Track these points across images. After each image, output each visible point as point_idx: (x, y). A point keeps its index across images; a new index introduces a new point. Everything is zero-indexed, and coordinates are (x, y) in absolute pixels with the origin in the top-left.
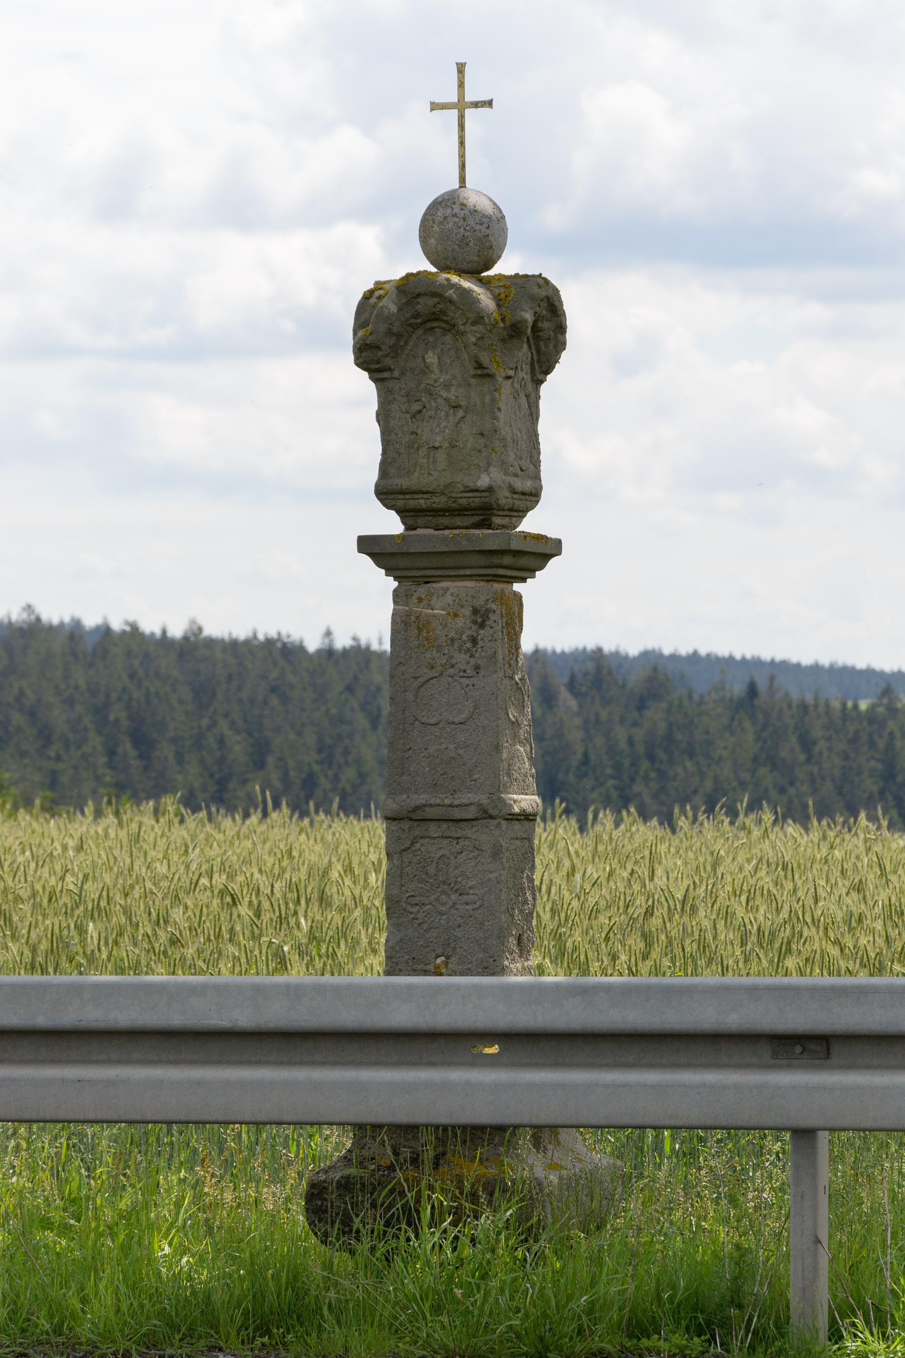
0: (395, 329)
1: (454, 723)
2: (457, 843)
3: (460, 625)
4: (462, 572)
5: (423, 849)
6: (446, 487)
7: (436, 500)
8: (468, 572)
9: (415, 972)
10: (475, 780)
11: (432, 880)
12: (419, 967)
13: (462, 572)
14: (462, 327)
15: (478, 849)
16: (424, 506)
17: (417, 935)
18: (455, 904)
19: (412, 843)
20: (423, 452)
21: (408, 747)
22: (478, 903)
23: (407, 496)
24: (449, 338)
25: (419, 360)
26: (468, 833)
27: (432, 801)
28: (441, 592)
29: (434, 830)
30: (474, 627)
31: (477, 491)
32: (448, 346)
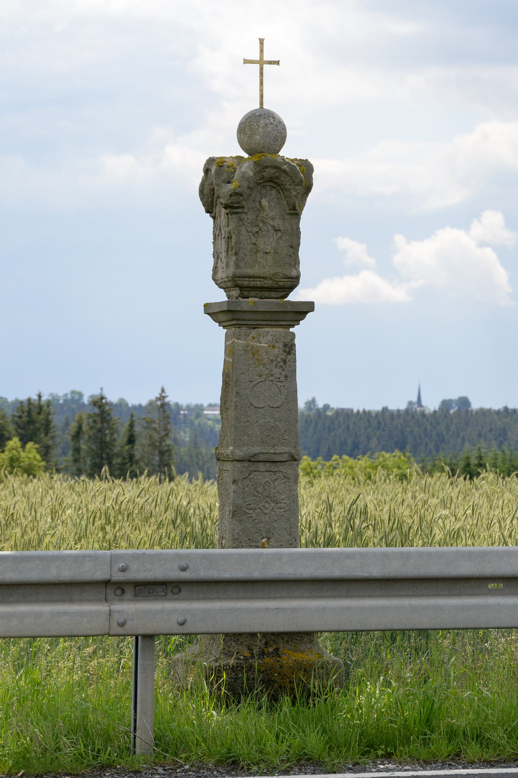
0: (251, 185)
1: (273, 407)
2: (274, 475)
3: (276, 352)
4: (280, 323)
5: (255, 477)
6: (274, 275)
7: (267, 282)
8: (283, 323)
9: (251, 547)
10: (285, 439)
11: (260, 495)
12: (253, 544)
13: (280, 323)
14: (288, 187)
15: (286, 478)
16: (259, 285)
17: (251, 526)
18: (273, 508)
19: (249, 475)
20: (259, 255)
21: (247, 420)
22: (287, 508)
23: (251, 279)
24: (274, 192)
25: (257, 204)
26: (282, 469)
27: (264, 451)
28: (265, 334)
29: (262, 467)
30: (284, 354)
31: (291, 278)
32: (273, 197)
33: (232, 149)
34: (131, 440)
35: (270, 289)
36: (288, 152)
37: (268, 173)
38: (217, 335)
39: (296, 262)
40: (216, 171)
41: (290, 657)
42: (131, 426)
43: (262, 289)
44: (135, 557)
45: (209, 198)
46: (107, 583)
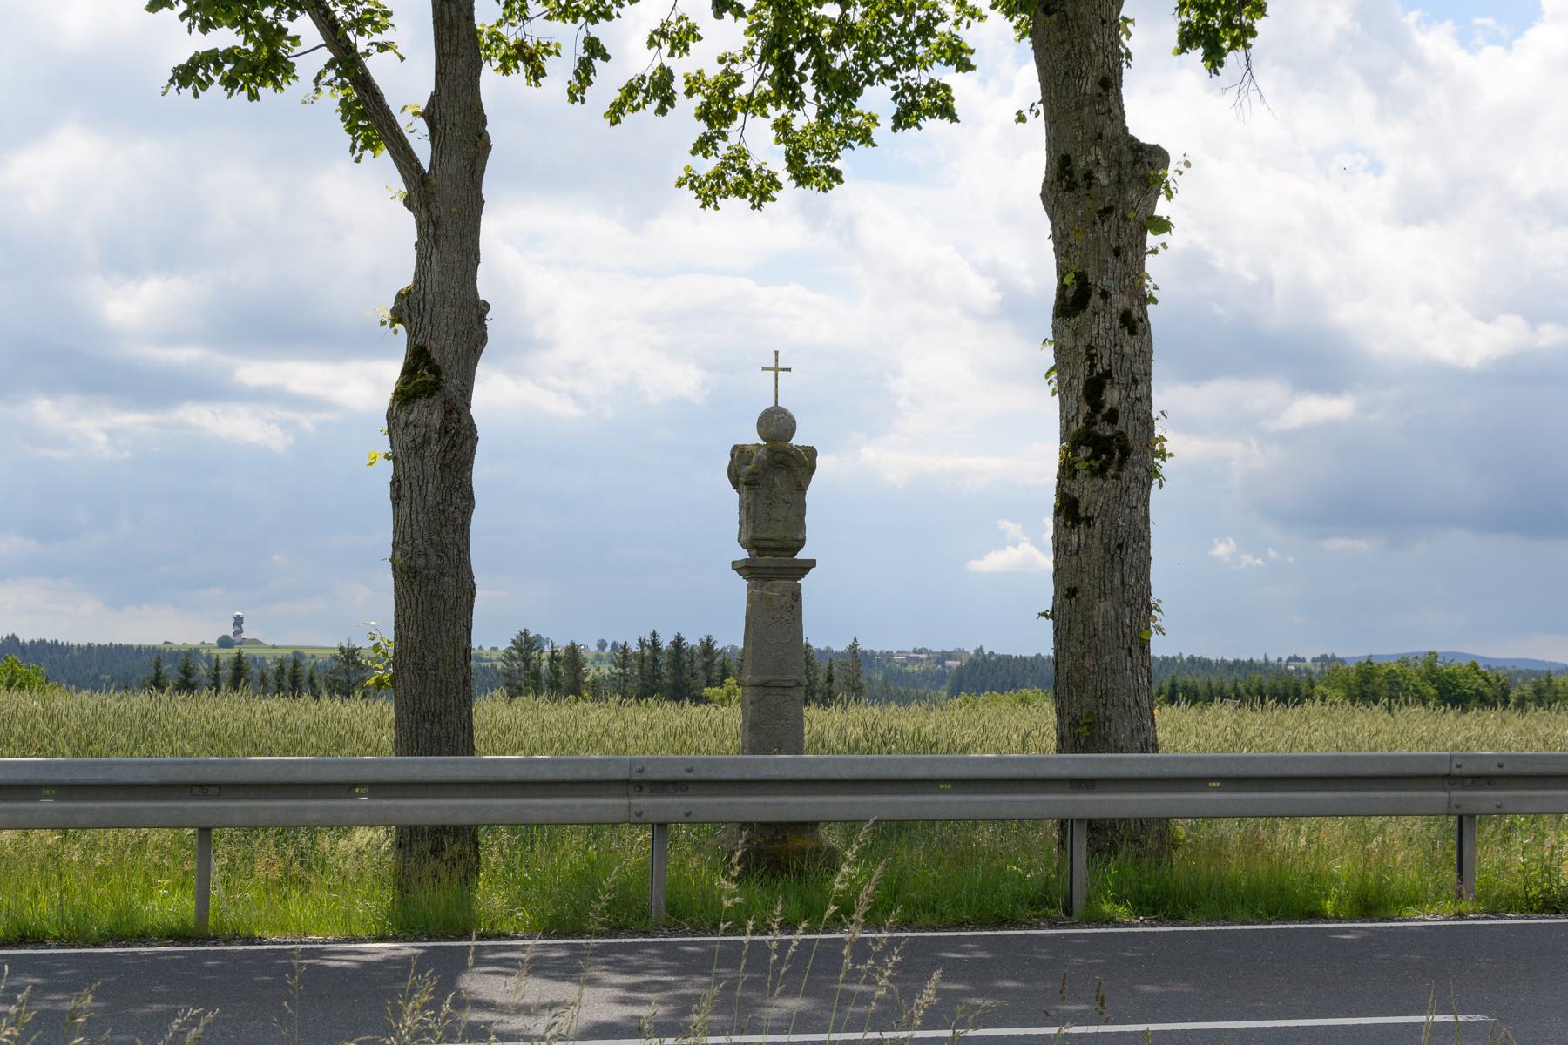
29: (774, 691)
33: (752, 438)
34: (830, 680)
35: (782, 549)
36: (796, 441)
37: (779, 457)
38: (741, 586)
39: (802, 527)
40: (740, 454)
41: (795, 842)
42: (830, 667)
43: (775, 549)
44: (650, 761)
45: (734, 477)
46: (628, 782)
